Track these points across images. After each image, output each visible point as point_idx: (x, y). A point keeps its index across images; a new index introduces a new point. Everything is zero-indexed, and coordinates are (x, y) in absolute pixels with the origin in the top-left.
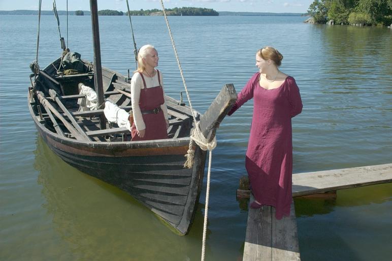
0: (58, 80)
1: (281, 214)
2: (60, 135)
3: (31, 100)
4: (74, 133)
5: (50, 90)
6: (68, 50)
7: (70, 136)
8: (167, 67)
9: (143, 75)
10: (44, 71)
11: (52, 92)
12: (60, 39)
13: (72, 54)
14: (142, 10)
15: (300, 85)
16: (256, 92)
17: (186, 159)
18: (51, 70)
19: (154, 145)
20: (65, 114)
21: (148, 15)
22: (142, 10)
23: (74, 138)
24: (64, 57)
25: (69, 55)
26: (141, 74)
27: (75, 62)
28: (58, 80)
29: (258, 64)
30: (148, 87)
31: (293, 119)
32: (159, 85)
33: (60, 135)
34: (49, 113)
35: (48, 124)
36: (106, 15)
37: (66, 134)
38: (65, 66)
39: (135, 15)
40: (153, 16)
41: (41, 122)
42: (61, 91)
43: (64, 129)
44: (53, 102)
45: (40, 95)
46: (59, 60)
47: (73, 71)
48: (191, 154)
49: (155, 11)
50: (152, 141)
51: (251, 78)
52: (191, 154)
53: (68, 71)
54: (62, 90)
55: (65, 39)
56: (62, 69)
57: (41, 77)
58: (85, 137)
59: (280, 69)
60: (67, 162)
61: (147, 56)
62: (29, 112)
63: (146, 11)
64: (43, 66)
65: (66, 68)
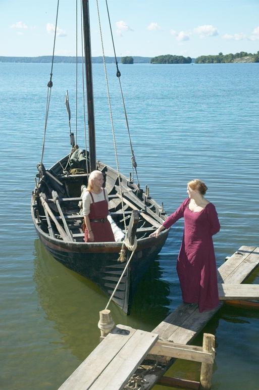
0: (62, 180)
1: (217, 322)
2: (51, 236)
3: (33, 202)
4: (62, 235)
5: (53, 191)
6: (77, 147)
7: (59, 236)
8: (242, 164)
9: (93, 194)
10: (51, 171)
11: (54, 194)
12: (70, 134)
13: (80, 150)
14: (221, 54)
15: (219, 211)
16: (185, 212)
17: (119, 256)
18: (57, 170)
19: (104, 246)
20: (60, 217)
21: (231, 62)
22: (221, 54)
23: (62, 239)
24: (72, 154)
25: (77, 153)
26: (90, 193)
27: (82, 161)
28: (62, 180)
29: (188, 191)
30: (95, 201)
31: (214, 237)
32: (104, 200)
33: (51, 236)
34: (47, 216)
35: (44, 226)
36: (165, 62)
37: (56, 235)
38: (72, 164)
39: (209, 62)
40: (238, 64)
41: (38, 224)
42: (66, 191)
43: (55, 230)
44: (52, 205)
45: (43, 197)
46: (67, 158)
47: (79, 171)
48: (123, 252)
49: (242, 55)
50: (102, 243)
51: (184, 201)
52: (123, 252)
53: (74, 169)
54: (67, 190)
55: (75, 136)
56: (68, 169)
57: (47, 177)
58: (70, 238)
59: (205, 197)
60: (55, 258)
61: (95, 178)
62: (31, 213)
63: (227, 56)
64: (49, 167)
65: (73, 167)
